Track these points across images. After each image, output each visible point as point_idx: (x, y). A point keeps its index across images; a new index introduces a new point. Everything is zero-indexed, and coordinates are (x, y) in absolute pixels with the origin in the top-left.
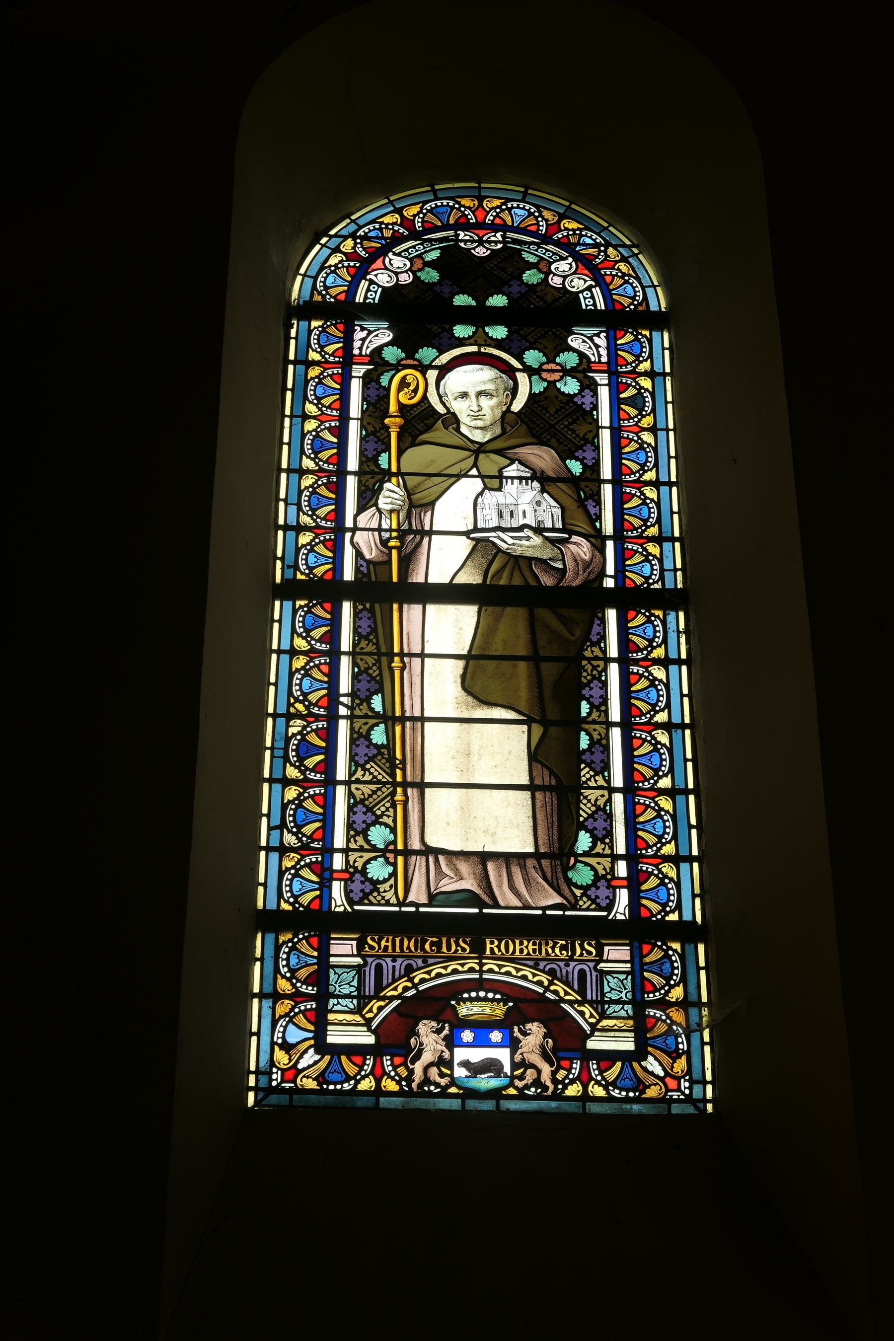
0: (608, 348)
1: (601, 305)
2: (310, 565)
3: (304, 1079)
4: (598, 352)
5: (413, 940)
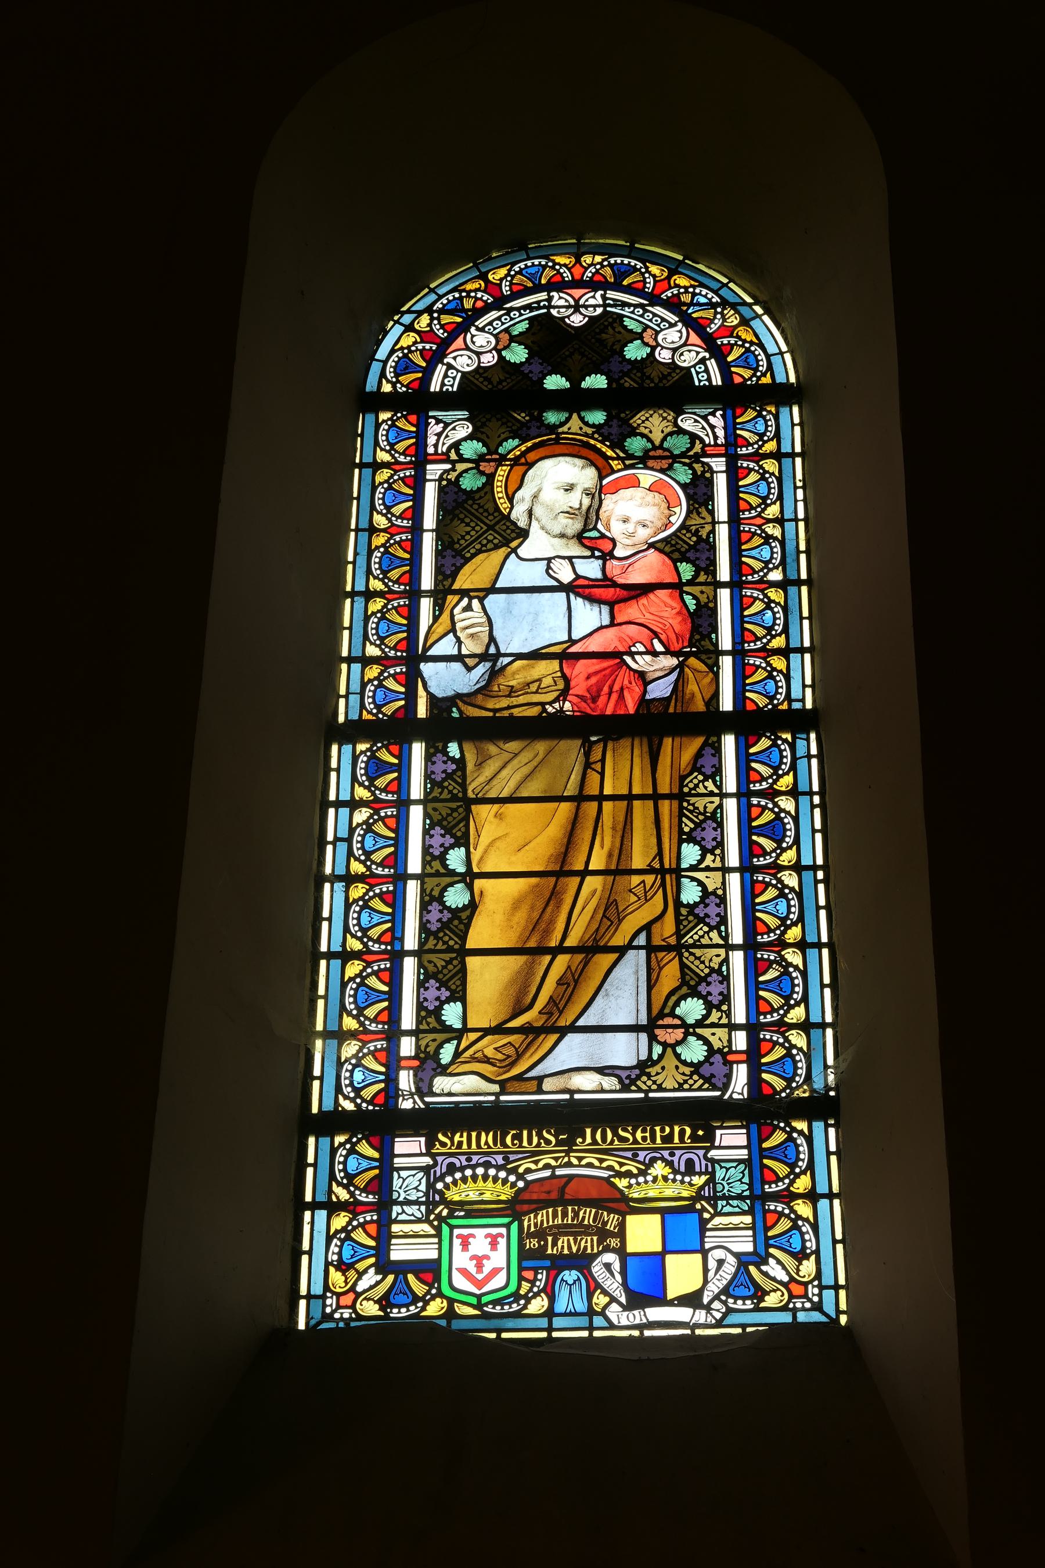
0: (725, 428)
1: (717, 380)
2: (388, 504)
3: (364, 1302)
4: (714, 433)
5: (491, 1134)
